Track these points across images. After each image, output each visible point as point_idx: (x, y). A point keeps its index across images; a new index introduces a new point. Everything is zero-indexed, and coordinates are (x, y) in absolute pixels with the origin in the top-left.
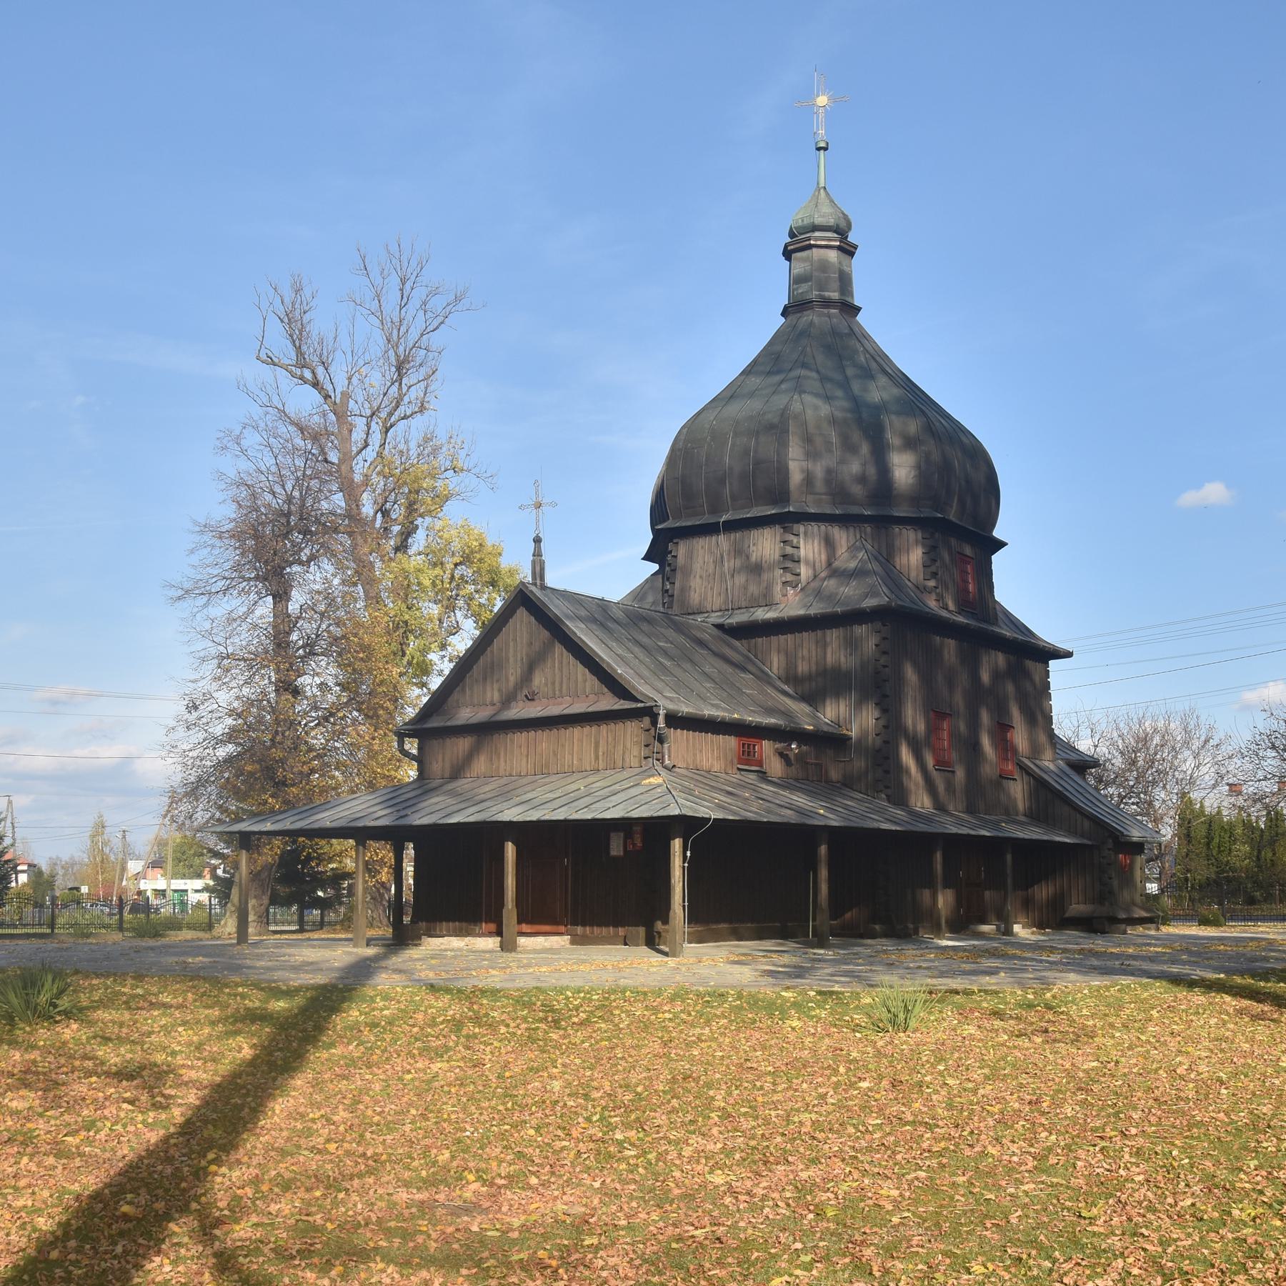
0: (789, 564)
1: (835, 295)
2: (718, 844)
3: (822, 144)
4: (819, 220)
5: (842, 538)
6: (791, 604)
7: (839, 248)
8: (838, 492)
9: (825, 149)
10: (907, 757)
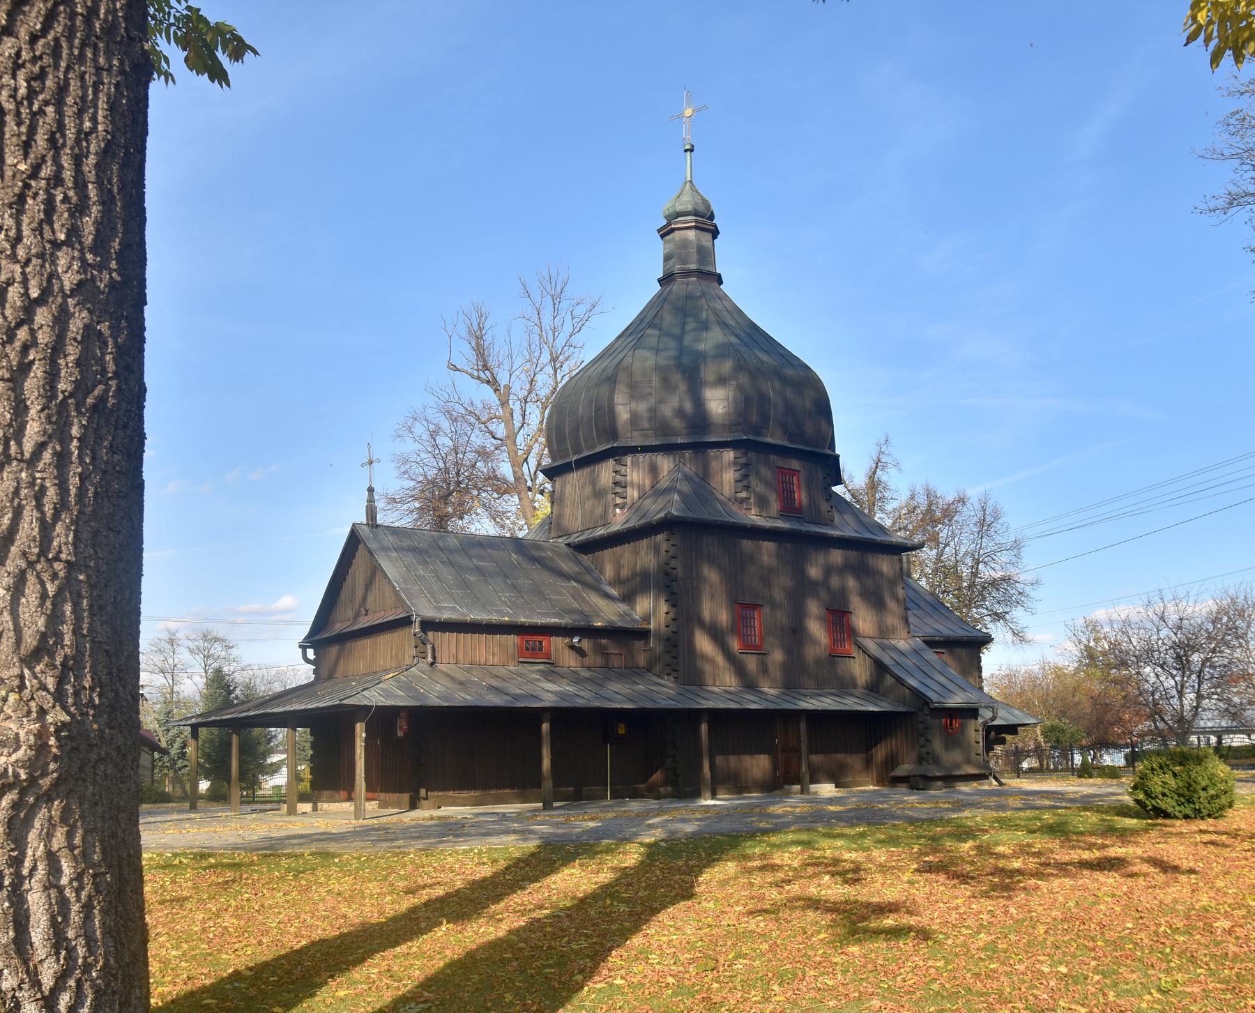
0: (619, 490)
1: (693, 267)
2: (568, 720)
3: (688, 147)
4: (679, 208)
5: (665, 464)
6: (619, 520)
7: (696, 228)
8: (663, 428)
9: (692, 150)
10: (704, 644)
